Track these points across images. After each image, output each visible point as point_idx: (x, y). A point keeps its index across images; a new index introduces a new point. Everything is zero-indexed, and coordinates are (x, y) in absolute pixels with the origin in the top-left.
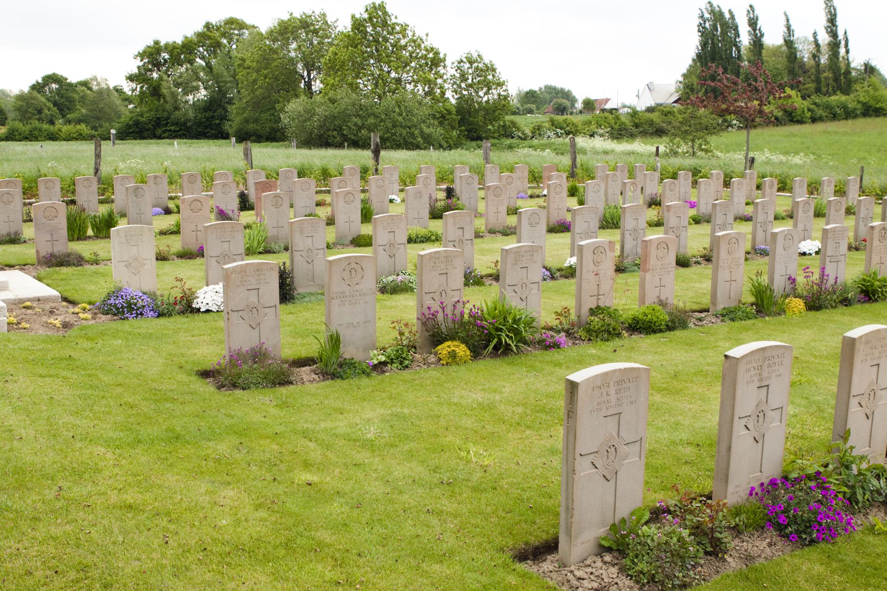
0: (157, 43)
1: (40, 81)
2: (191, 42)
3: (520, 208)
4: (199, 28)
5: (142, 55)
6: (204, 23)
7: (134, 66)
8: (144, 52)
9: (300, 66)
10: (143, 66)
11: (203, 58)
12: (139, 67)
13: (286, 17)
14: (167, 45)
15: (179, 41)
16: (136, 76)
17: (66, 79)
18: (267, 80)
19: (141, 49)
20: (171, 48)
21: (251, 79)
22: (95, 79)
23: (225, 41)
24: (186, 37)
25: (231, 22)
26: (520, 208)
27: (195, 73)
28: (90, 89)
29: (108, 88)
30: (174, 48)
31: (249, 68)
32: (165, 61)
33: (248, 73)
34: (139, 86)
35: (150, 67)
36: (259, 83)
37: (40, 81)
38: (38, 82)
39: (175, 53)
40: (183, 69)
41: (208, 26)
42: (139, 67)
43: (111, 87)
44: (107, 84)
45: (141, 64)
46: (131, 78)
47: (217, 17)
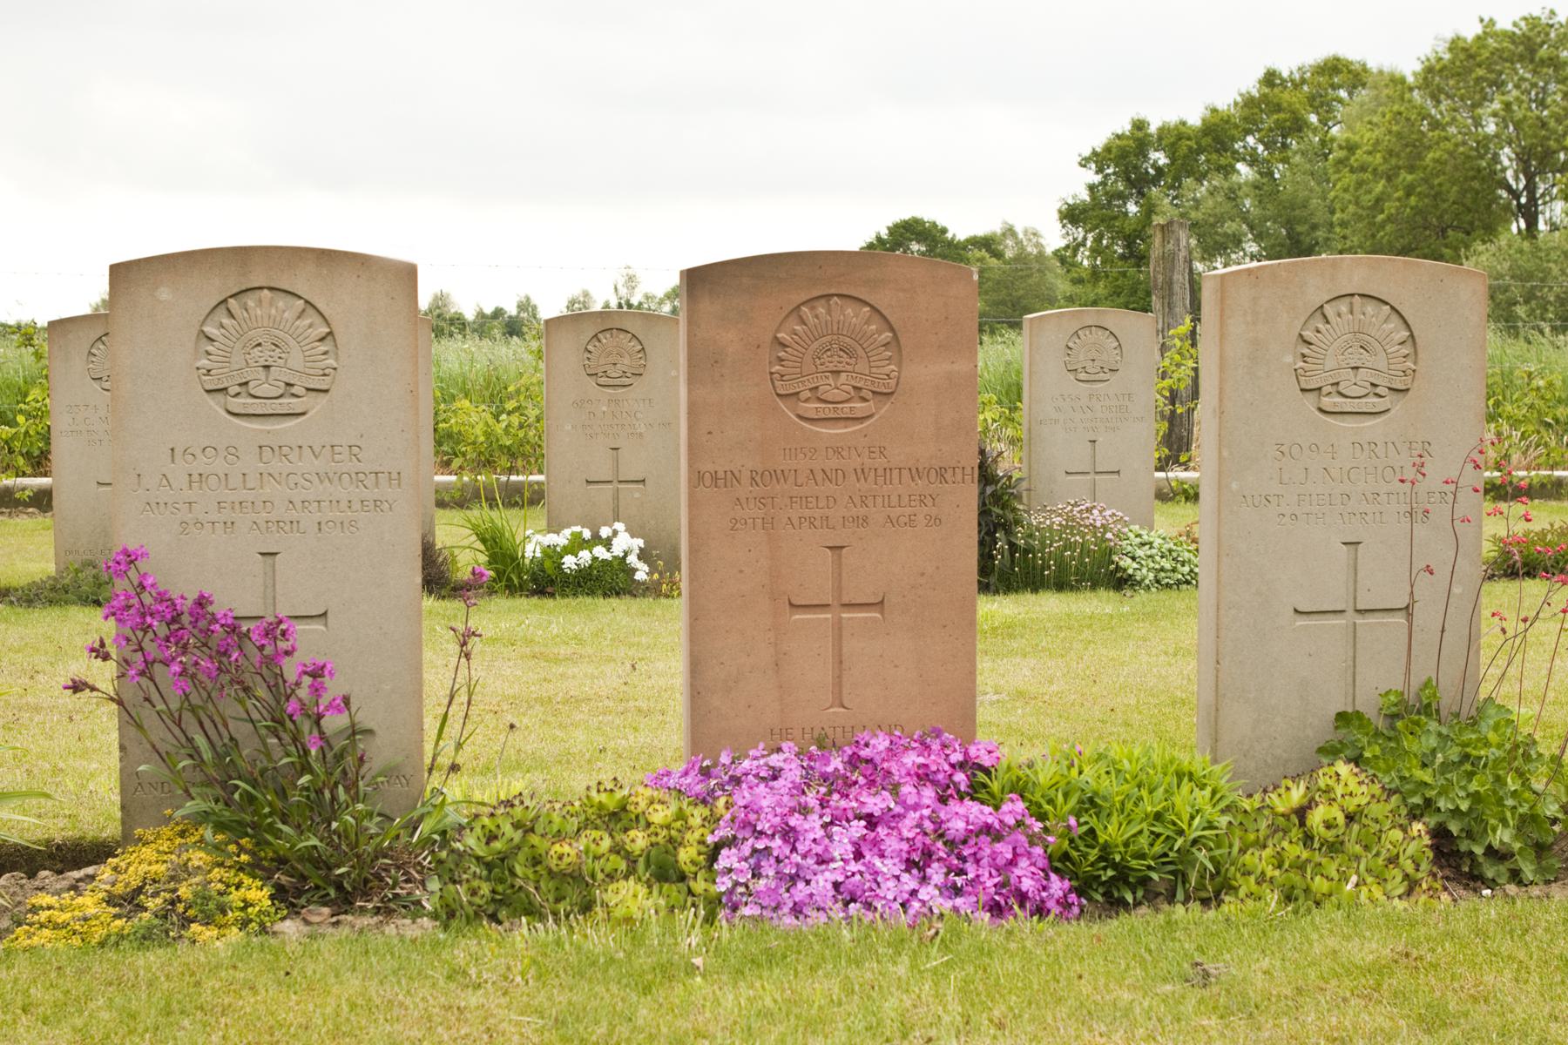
0: (1139, 125)
1: (884, 234)
2: (1227, 120)
3: (1039, 920)
4: (1250, 83)
5: (1098, 159)
6: (1260, 73)
7: (1078, 184)
8: (1108, 149)
9: (1506, 155)
10: (1103, 184)
11: (1253, 161)
12: (1092, 188)
13: (1471, 31)
14: (1163, 131)
15: (1195, 120)
16: (1084, 211)
17: (944, 231)
18: (1413, 200)
19: (1099, 141)
20: (1173, 138)
21: (1367, 200)
22: (1010, 232)
23: (1313, 118)
24: (1214, 111)
25: (1333, 67)
26: (1039, 920)
27: (1232, 195)
28: (998, 255)
29: (1041, 254)
30: (1180, 137)
31: (1363, 169)
32: (1159, 170)
33: (1360, 184)
34: (1090, 236)
35: (1120, 186)
36: (1390, 207)
37: (884, 234)
38: (879, 238)
39: (1183, 150)
40: (1202, 191)
41: (1270, 78)
42: (1092, 188)
43: (1049, 251)
44: (1038, 245)
45: (1098, 178)
46: (1072, 215)
47: (1295, 56)
